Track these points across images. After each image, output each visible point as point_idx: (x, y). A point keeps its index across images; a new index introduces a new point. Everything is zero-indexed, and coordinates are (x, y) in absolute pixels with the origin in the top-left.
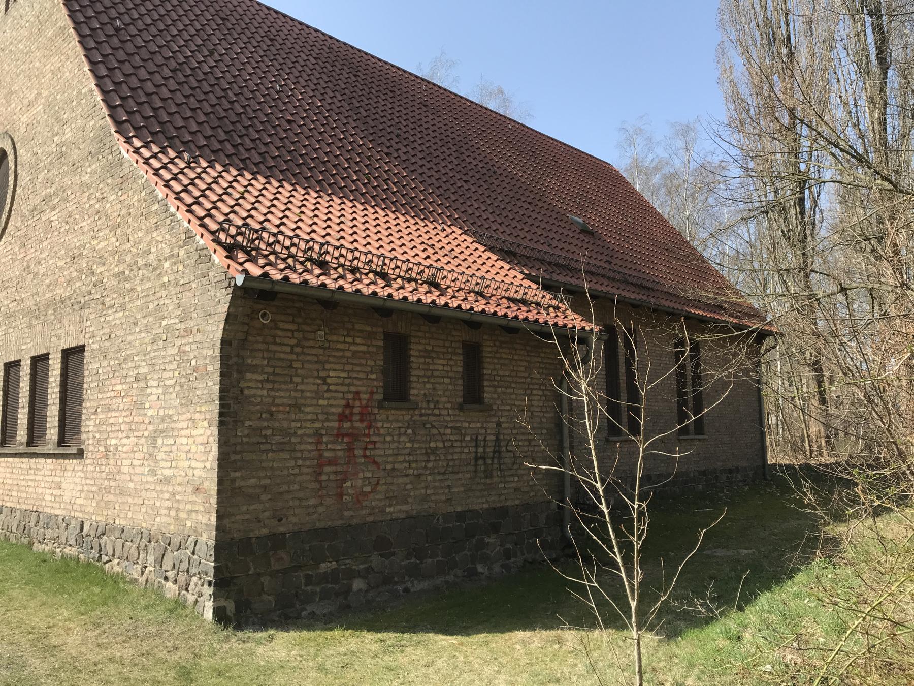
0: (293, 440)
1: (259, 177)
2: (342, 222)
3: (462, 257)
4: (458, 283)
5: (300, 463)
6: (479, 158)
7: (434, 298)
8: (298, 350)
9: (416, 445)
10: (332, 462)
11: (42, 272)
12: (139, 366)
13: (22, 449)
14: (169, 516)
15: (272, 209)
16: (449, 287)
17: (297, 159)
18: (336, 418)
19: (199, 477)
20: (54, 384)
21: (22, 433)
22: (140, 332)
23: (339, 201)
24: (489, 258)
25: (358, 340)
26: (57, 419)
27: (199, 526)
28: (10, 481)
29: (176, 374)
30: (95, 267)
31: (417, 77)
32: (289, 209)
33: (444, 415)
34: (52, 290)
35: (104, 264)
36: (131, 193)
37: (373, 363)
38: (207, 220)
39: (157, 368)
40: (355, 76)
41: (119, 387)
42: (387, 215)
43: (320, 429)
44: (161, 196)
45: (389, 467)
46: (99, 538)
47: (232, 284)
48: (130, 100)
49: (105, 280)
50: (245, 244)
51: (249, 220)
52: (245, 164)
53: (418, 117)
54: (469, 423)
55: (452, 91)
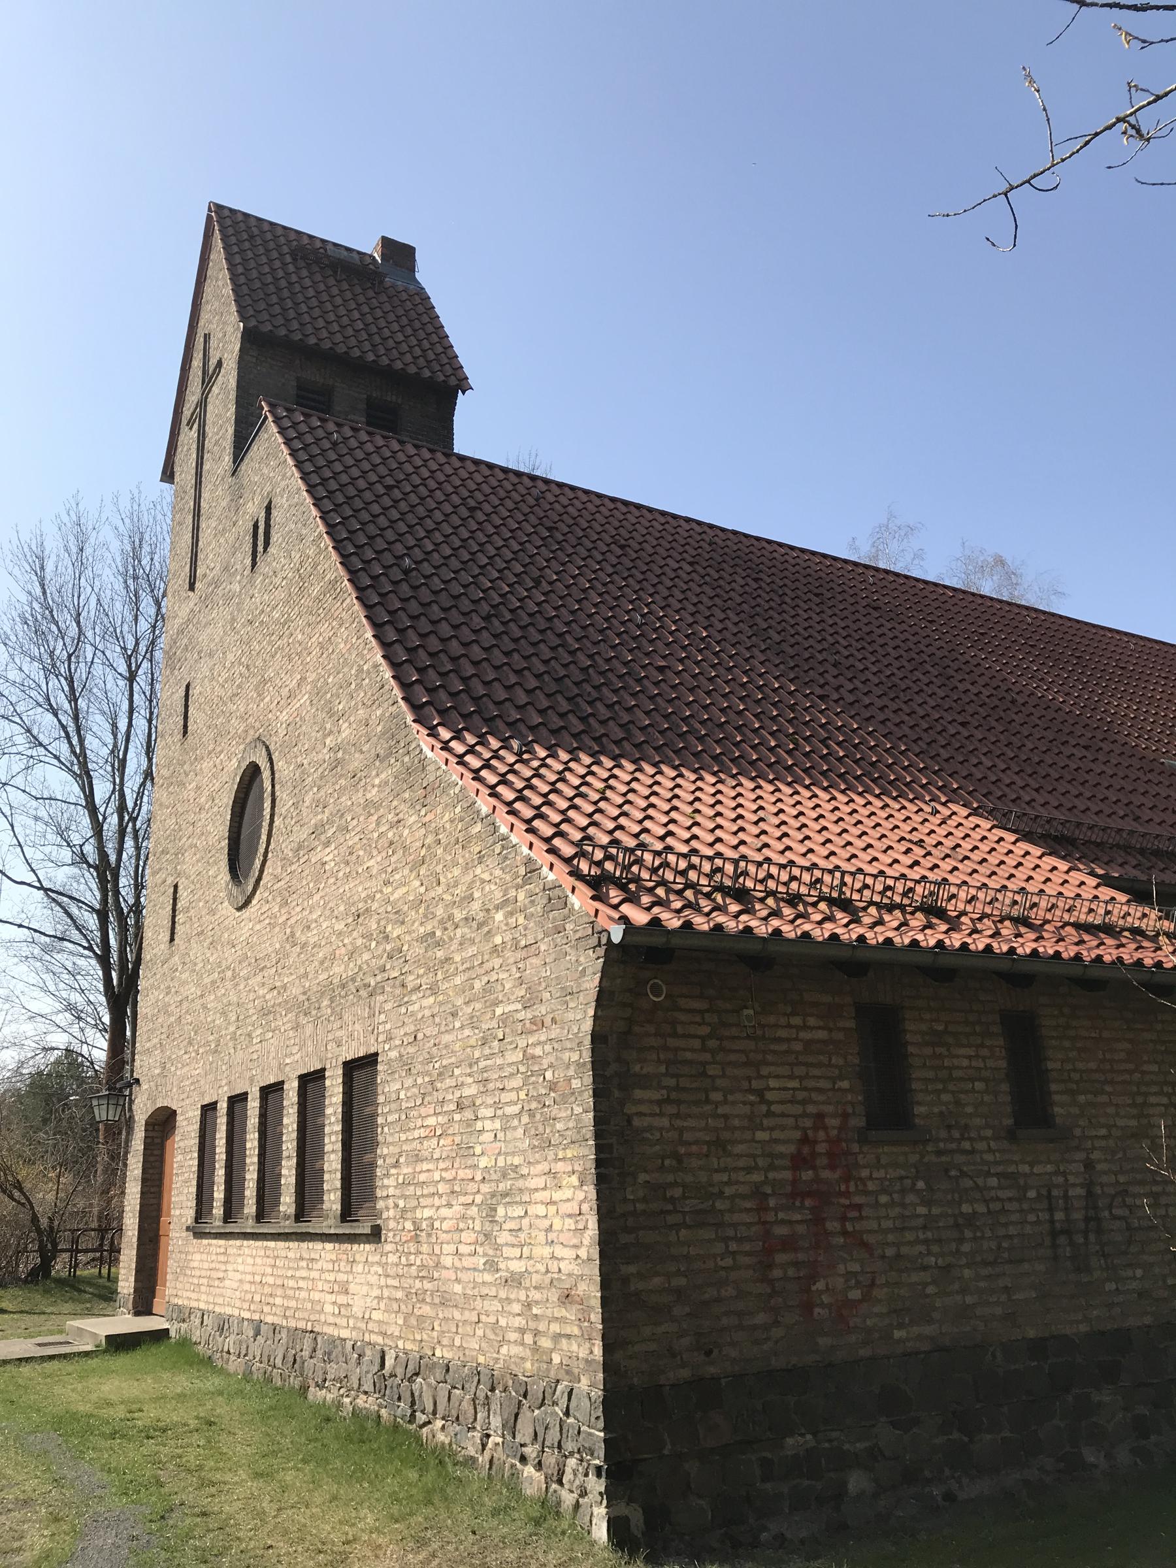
0: (719, 1205)
1: (624, 762)
2: (762, 819)
3: (976, 856)
4: (979, 906)
5: (733, 1246)
6: (982, 681)
7: (941, 937)
8: (712, 1044)
9: (936, 1211)
10: (788, 1244)
11: (312, 941)
12: (462, 1084)
13: (288, 1226)
14: (523, 1344)
15: (651, 812)
16: (964, 913)
17: (678, 726)
18: (786, 1162)
19: (569, 1275)
20: (333, 1119)
21: (288, 1200)
22: (462, 1027)
23: (752, 785)
24: (1027, 853)
25: (812, 1021)
26: (339, 1175)
27: (574, 1363)
28: (271, 1280)
29: (522, 1095)
30: (389, 928)
31: (856, 564)
32: (675, 808)
33: (981, 1152)
34: (327, 969)
35: (403, 923)
36: (439, 810)
37: (841, 1062)
38: (557, 842)
39: (491, 1086)
40: (756, 580)
41: (431, 1121)
42: (834, 798)
43: (764, 1183)
44: (485, 810)
45: (890, 1252)
46: (411, 1380)
47: (604, 941)
48: (431, 671)
49: (405, 948)
50: (618, 874)
51: (618, 834)
52: (601, 745)
53: (866, 629)
54: (1031, 1165)
55: (947, 583)
